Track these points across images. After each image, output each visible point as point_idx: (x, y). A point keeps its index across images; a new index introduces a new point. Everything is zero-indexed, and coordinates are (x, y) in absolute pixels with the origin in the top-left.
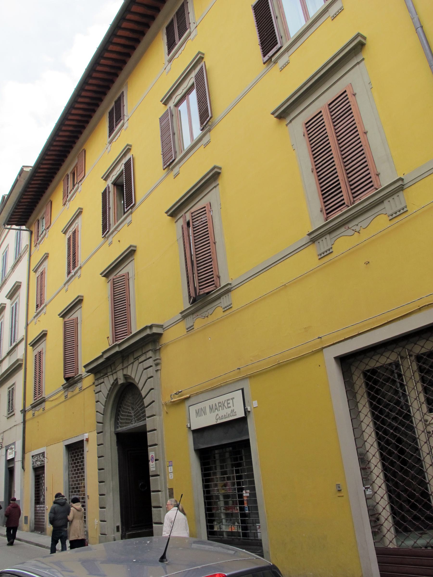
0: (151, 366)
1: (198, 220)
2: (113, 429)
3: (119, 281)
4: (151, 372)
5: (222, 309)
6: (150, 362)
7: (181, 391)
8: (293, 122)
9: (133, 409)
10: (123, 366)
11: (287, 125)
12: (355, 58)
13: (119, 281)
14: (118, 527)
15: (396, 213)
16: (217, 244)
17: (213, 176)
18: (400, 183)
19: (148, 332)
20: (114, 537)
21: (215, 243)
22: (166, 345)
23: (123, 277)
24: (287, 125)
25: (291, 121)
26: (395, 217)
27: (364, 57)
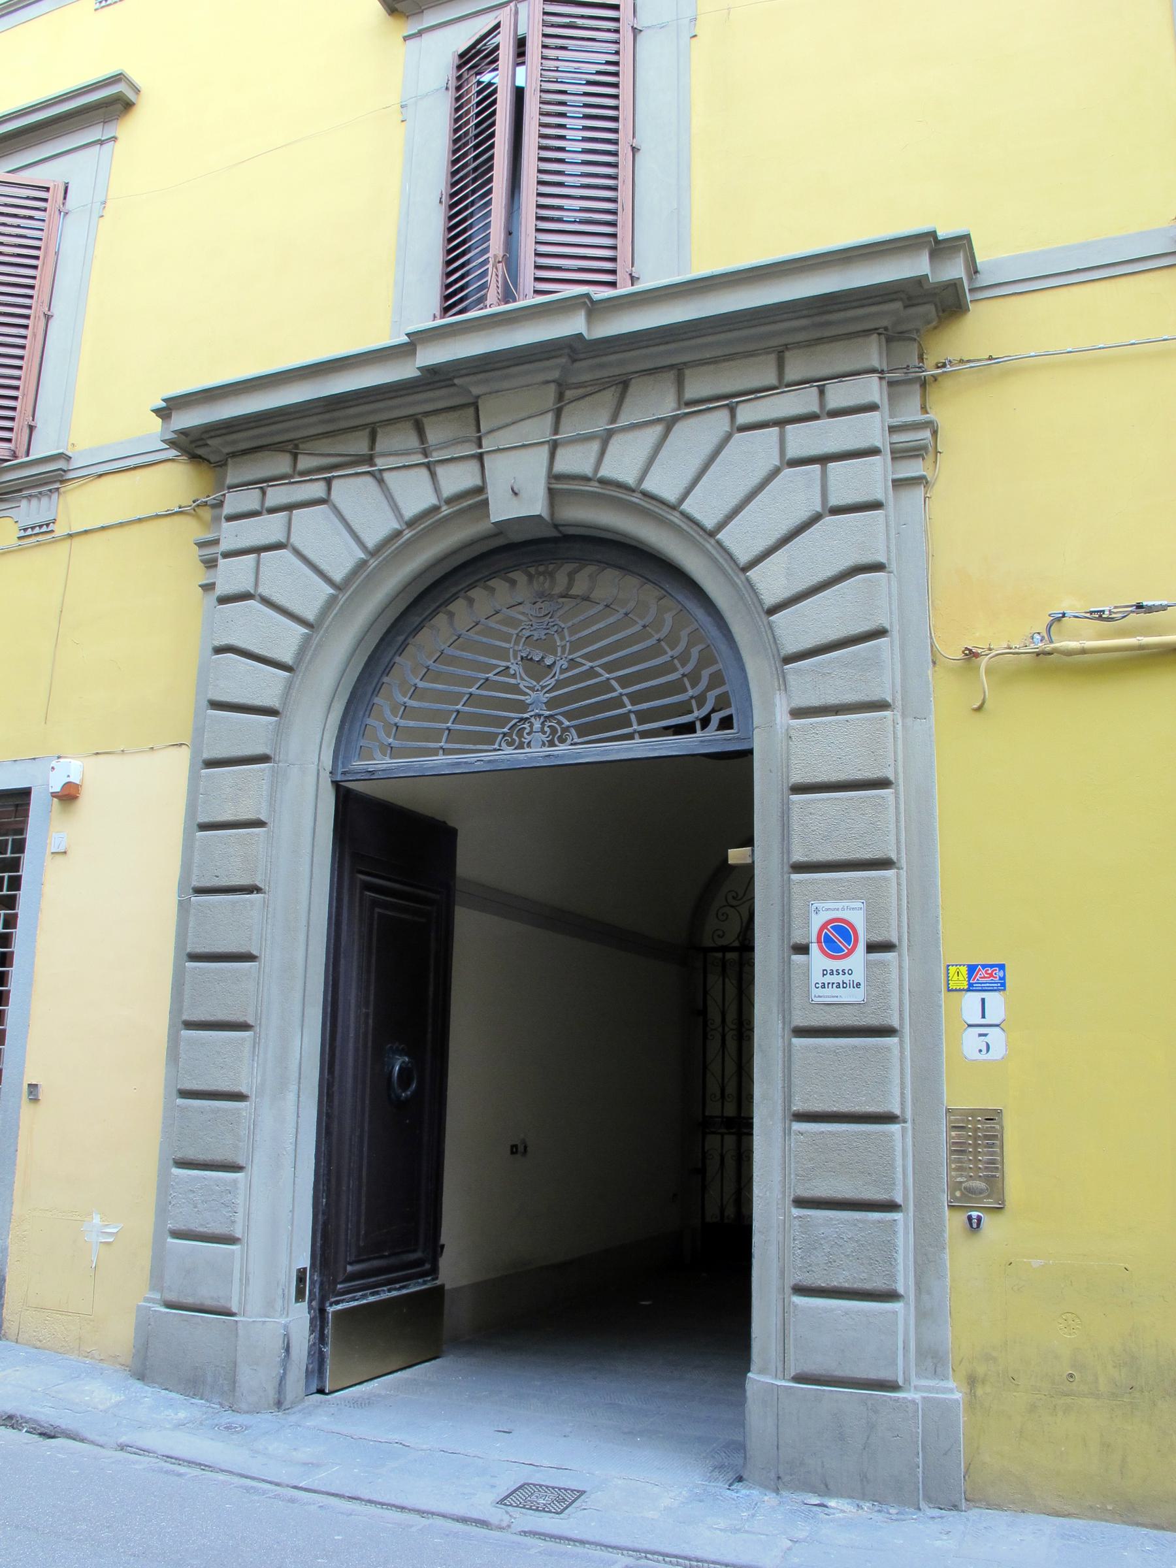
0: (874, 452)
1: (31, 218)
2: (328, 763)
3: (580, 22)
4: (868, 480)
5: (16, 527)
6: (870, 429)
7: (1163, 608)
8: (426, 37)
9: (536, 669)
10: (614, 419)
11: (406, 38)
12: (100, 126)
13: (580, 22)
14: (301, 1277)
15: (40, 527)
16: (53, 324)
17: (104, 106)
18: (61, 464)
19: (918, 266)
20: (286, 1327)
21: (48, 318)
22: (994, 367)
23: (43, 195)
24: (406, 38)
25: (420, 33)
26: (30, 536)
27: (117, 135)
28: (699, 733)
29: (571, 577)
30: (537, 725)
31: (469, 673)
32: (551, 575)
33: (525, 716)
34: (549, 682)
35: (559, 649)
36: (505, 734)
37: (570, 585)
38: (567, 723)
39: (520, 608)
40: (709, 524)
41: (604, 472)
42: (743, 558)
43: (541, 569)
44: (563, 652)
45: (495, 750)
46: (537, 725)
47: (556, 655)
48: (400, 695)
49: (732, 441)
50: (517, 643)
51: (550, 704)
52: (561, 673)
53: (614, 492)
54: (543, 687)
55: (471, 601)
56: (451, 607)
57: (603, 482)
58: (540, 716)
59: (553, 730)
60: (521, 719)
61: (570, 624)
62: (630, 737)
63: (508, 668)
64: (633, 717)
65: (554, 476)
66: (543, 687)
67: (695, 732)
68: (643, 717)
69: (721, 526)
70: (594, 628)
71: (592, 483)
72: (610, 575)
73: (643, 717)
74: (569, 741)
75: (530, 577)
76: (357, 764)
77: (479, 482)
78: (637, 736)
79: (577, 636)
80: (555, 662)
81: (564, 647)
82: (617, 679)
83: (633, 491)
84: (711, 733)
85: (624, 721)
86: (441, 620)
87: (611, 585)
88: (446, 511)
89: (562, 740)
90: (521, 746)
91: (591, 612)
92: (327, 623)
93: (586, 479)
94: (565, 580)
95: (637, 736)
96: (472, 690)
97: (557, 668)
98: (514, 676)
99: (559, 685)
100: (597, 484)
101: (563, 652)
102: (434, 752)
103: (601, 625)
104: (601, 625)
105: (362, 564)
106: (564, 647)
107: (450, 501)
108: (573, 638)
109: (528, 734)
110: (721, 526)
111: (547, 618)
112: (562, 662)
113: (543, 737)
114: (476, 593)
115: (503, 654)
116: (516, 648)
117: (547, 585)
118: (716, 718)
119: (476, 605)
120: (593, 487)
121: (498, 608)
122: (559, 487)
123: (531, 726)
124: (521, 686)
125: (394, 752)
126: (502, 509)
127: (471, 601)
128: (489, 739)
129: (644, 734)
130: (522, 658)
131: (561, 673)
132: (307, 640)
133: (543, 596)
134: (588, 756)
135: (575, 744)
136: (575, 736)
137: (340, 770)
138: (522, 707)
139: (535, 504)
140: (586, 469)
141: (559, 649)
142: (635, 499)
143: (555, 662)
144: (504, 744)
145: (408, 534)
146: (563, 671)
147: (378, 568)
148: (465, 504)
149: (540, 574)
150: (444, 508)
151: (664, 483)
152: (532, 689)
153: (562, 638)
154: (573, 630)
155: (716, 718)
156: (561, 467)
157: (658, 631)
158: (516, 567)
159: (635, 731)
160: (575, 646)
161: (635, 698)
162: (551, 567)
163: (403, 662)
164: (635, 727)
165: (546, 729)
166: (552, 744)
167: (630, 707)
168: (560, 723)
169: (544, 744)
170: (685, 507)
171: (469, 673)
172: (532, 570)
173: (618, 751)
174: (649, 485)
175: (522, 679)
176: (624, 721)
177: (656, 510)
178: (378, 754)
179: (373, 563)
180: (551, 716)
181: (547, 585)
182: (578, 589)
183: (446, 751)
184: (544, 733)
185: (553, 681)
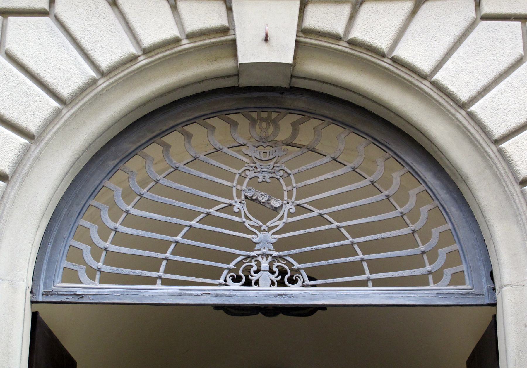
28: (432, 286)
29: (295, 126)
30: (265, 264)
31: (188, 206)
32: (275, 123)
33: (252, 254)
34: (276, 223)
35: (286, 194)
36: (230, 270)
37: (294, 135)
38: (296, 265)
39: (243, 149)
40: (464, 96)
41: (356, 34)
42: (498, 132)
43: (264, 115)
44: (290, 197)
45: (220, 284)
46: (265, 264)
47: (282, 199)
48: (109, 220)
49: (477, 29)
50: (240, 183)
51: (278, 245)
52: (288, 217)
53: (364, 55)
54: (270, 229)
55: (188, 136)
56: (167, 139)
57: (353, 43)
58: (267, 256)
59: (283, 273)
60: (248, 257)
61: (296, 171)
62: (363, 283)
63: (230, 205)
64: (365, 265)
65: (303, 31)
66: (270, 229)
67: (427, 284)
68: (375, 266)
69: (474, 100)
70: (322, 178)
71: (341, 43)
72: (334, 130)
73: (375, 266)
74: (300, 282)
75: (253, 122)
76: (60, 286)
77: (225, 22)
78: (370, 283)
79: (303, 184)
80: (282, 206)
81: (290, 193)
82: (346, 228)
83: (383, 55)
84: (444, 286)
85: (356, 268)
86: (154, 150)
87: (338, 140)
88: (186, 44)
89: (292, 281)
90: (248, 283)
91: (318, 163)
92: (48, 136)
93: (337, 38)
94: (290, 130)
95: (370, 283)
96: (193, 223)
97: (285, 211)
98: (238, 214)
99: (287, 227)
100: (346, 44)
101: (290, 197)
102: (152, 281)
103: (329, 176)
104: (329, 176)
105: (92, 83)
106: (290, 193)
107: (191, 36)
108: (300, 185)
109: (256, 272)
110: (474, 100)
111: (272, 163)
112: (289, 206)
113: (273, 277)
114: (193, 129)
115: (227, 192)
116: (239, 187)
117: (270, 131)
118: (448, 273)
119: (194, 141)
120: (343, 46)
121: (219, 146)
122: (307, 39)
123: (259, 264)
124: (246, 224)
125: (106, 278)
126: (251, 52)
127: (188, 136)
128: (215, 273)
129: (377, 283)
130: (246, 197)
131: (288, 217)
132: (27, 150)
133: (265, 141)
134: (323, 298)
135: (307, 286)
136: (306, 279)
137: (42, 291)
138: (250, 245)
139: (283, 53)
140: (339, 28)
141: (286, 194)
142: (385, 63)
143: (282, 206)
144: (229, 280)
145: (143, 61)
146: (290, 215)
147: (108, 89)
148: (208, 41)
149: (262, 120)
150: (184, 41)
151: (418, 52)
152: (259, 228)
153: (288, 184)
154: (300, 177)
155: (448, 273)
156: (310, 22)
157: (387, 188)
158: (237, 110)
159: (369, 279)
160: (303, 193)
161: (366, 248)
162: (274, 115)
163: (115, 186)
164: (161, 273)
165: (275, 269)
166: (281, 283)
167: (361, 256)
168: (290, 264)
169: (273, 283)
170: (438, 77)
171: (188, 206)
172: (255, 115)
173: (355, 296)
174: (403, 52)
175: (247, 218)
176: (356, 268)
177: (407, 77)
178: (83, 276)
179: (103, 84)
180: (281, 257)
181: (270, 131)
182: (303, 139)
183: (166, 282)
184: (273, 272)
185: (281, 224)
